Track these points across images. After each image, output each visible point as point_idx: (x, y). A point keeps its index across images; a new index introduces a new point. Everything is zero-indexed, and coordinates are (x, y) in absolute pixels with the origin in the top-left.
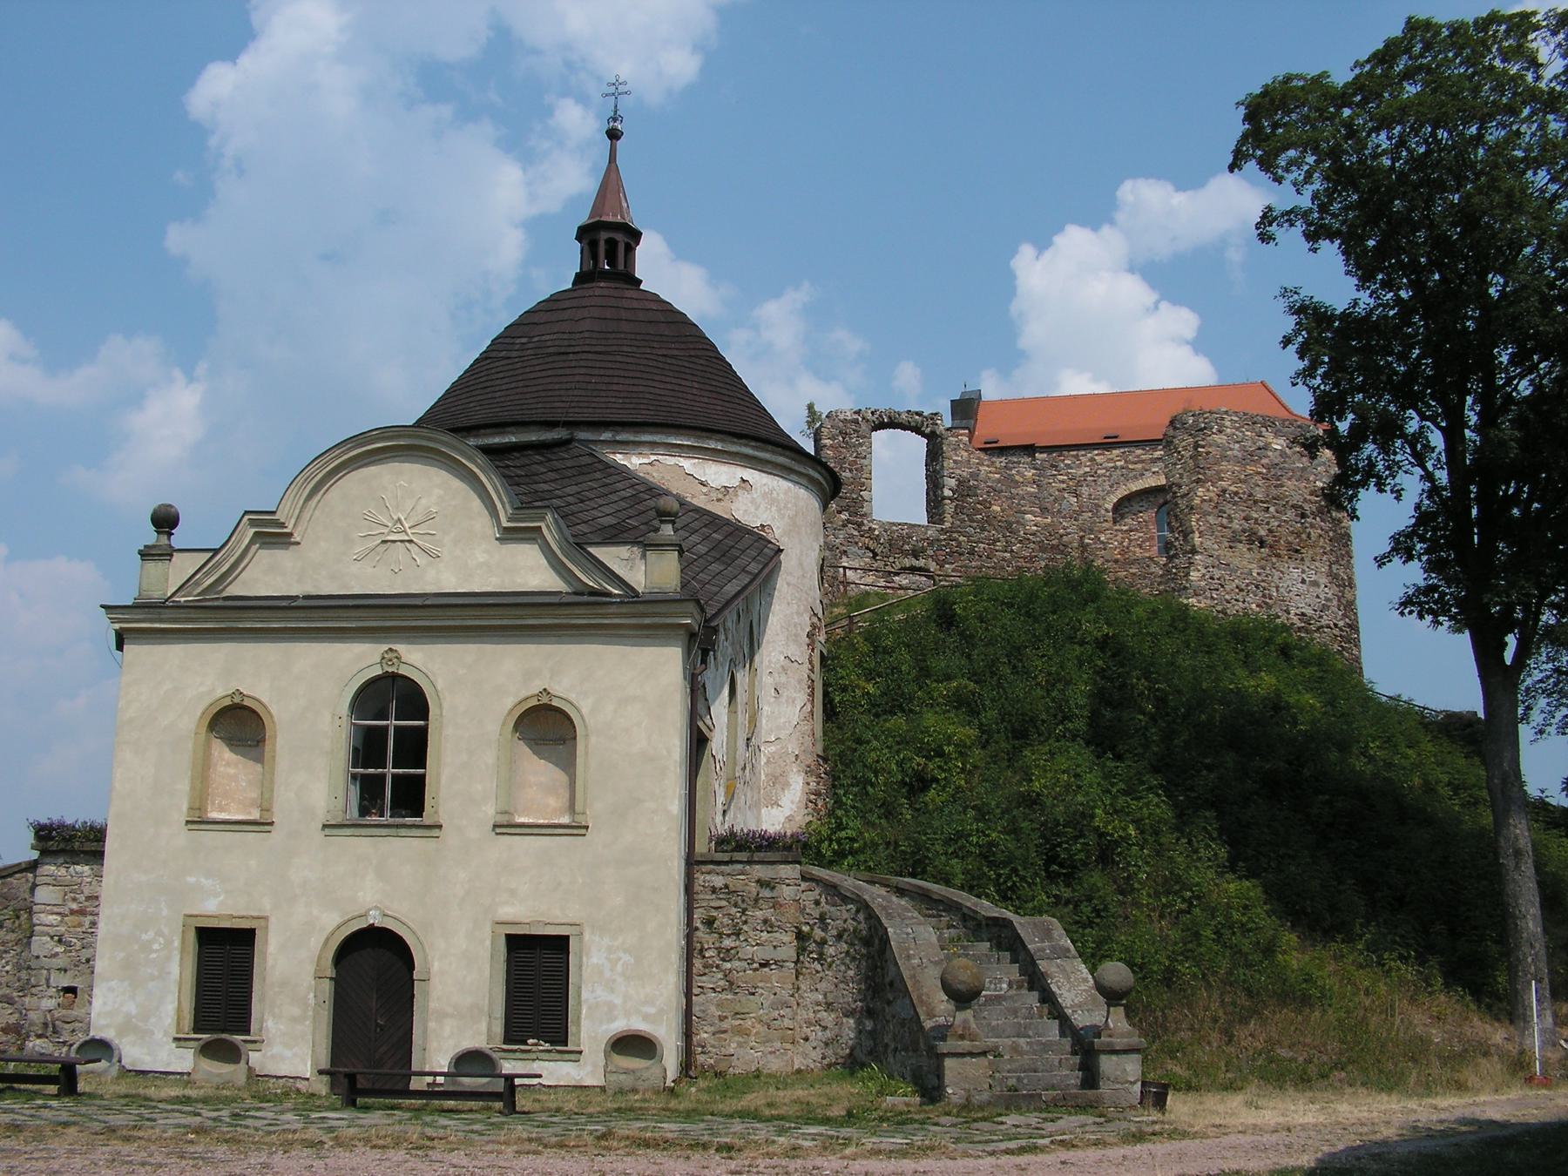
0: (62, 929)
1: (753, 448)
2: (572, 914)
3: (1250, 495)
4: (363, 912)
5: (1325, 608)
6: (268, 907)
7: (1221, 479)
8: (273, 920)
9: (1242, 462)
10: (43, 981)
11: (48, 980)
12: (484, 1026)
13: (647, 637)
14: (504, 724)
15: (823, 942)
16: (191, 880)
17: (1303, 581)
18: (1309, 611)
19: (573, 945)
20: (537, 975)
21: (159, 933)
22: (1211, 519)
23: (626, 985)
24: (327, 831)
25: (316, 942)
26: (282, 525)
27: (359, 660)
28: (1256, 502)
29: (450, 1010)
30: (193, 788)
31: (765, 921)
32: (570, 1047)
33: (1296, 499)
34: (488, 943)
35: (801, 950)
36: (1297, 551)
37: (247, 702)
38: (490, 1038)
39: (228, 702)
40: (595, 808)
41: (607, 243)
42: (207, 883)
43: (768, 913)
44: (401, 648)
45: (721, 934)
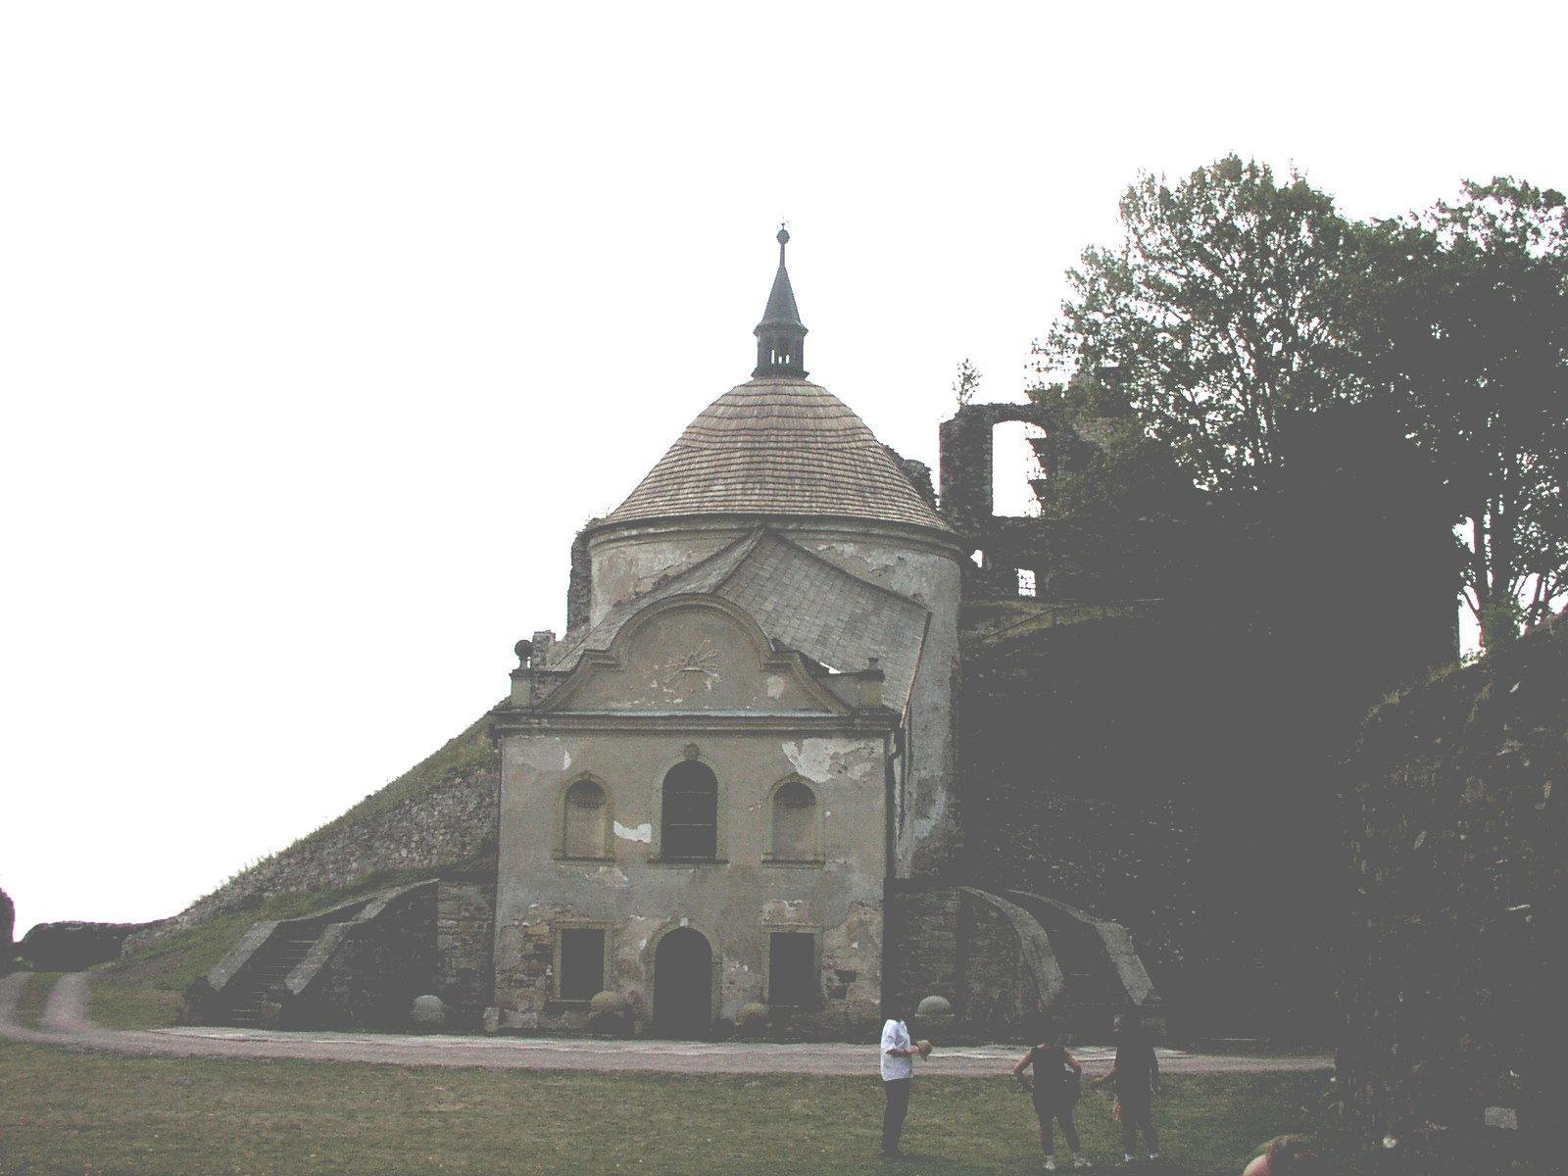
41: (781, 335)
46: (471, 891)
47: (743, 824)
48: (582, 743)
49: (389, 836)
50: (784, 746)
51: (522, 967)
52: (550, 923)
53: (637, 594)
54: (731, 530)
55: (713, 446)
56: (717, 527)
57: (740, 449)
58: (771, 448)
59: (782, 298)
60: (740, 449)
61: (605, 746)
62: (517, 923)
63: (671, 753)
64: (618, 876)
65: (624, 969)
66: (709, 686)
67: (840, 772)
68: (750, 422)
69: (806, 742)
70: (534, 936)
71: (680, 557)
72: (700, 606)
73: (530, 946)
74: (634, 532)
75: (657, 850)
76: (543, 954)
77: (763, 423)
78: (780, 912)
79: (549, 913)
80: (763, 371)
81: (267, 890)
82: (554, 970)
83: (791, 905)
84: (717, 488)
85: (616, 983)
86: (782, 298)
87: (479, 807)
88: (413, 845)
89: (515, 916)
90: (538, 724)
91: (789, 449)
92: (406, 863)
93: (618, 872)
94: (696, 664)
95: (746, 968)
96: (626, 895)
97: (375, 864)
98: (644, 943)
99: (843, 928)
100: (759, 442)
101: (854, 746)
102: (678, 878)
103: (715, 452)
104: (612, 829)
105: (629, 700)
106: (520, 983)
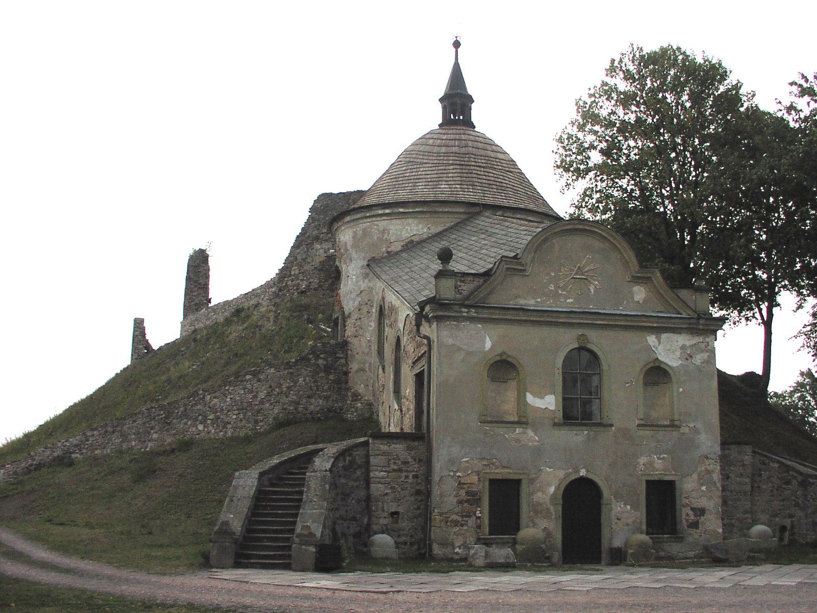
20: (661, 498)
37: (509, 359)
39: (498, 358)
41: (457, 102)
47: (620, 397)
48: (501, 329)
49: (185, 415)
50: (648, 338)
51: (456, 510)
52: (478, 473)
53: (388, 252)
54: (460, 213)
55: (431, 162)
56: (450, 210)
57: (452, 164)
58: (473, 166)
59: (457, 78)
60: (452, 164)
61: (517, 332)
62: (452, 474)
63: (568, 340)
64: (531, 436)
65: (538, 511)
66: (592, 291)
67: (687, 359)
68: (454, 149)
69: (664, 336)
70: (464, 484)
71: (422, 229)
72: (586, 230)
73: (463, 493)
74: (387, 211)
75: (560, 415)
76: (473, 499)
77: (463, 150)
78: (651, 463)
79: (479, 466)
80: (447, 122)
81: (74, 452)
82: (483, 512)
83: (659, 459)
84: (443, 186)
85: (532, 521)
86: (457, 78)
87: (269, 394)
88: (209, 422)
89: (452, 468)
90: (467, 312)
91: (484, 167)
92: (203, 434)
93: (530, 433)
94: (582, 274)
95: (629, 507)
96: (538, 452)
97: (174, 435)
98: (552, 489)
99: (695, 476)
100: (464, 161)
101: (696, 340)
102: (575, 437)
103: (432, 165)
104: (525, 398)
105: (533, 298)
106: (456, 523)
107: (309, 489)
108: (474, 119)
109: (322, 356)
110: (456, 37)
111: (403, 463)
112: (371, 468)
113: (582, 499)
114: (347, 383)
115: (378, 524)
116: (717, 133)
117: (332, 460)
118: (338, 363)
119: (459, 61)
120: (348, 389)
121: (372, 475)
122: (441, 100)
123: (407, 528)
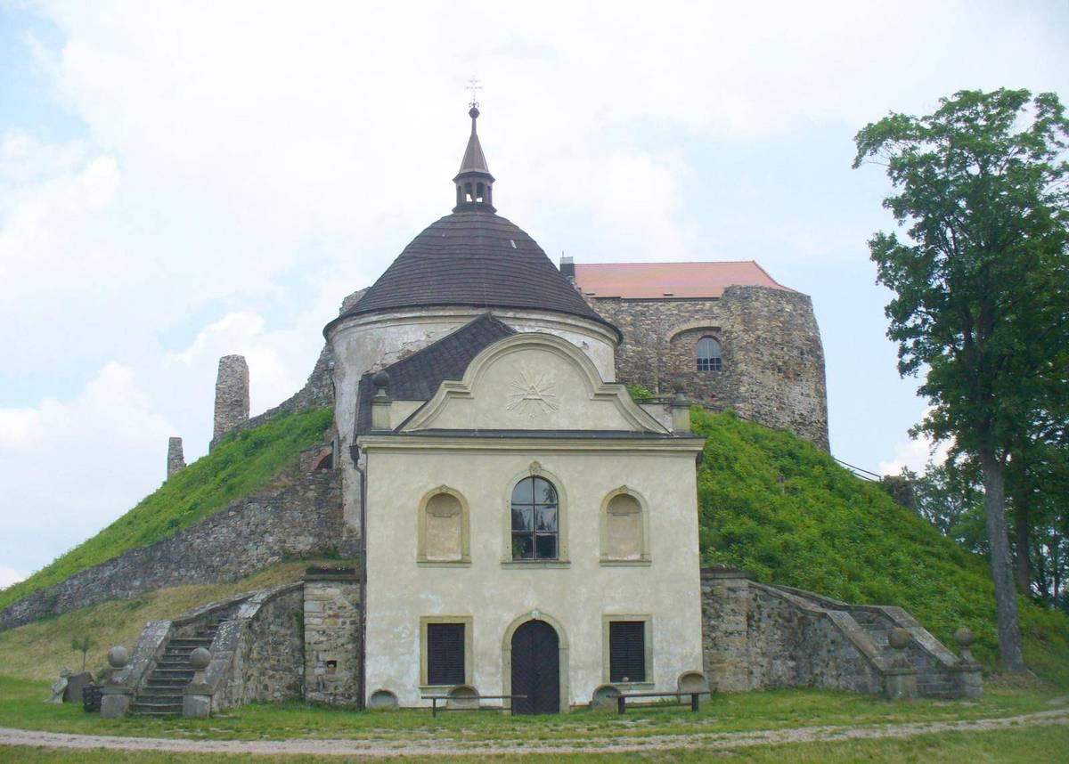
0: (324, 627)
1: (590, 324)
2: (646, 611)
3: (773, 340)
4: (527, 612)
5: (813, 410)
6: (471, 611)
7: (757, 330)
8: (475, 618)
9: (769, 319)
10: (314, 658)
11: (317, 658)
12: (600, 673)
13: (678, 457)
14: (602, 505)
15: (760, 620)
16: (423, 596)
17: (802, 394)
18: (805, 413)
19: (466, 626)
20: (627, 644)
21: (406, 628)
22: (751, 354)
23: (676, 650)
24: (421, 565)
25: (501, 631)
26: (465, 388)
27: (515, 467)
28: (776, 344)
29: (581, 665)
30: (420, 542)
31: (732, 610)
32: (648, 682)
33: (799, 343)
34: (600, 626)
35: (749, 625)
36: (799, 375)
37: (450, 492)
38: (604, 679)
39: (438, 492)
40: (655, 552)
41: (474, 180)
42: (433, 598)
43: (733, 606)
44: (541, 460)
45: (709, 618)
46: (335, 592)
47: (581, 526)
59: (474, 151)
80: (462, 207)
86: (474, 151)
94: (537, 394)
107: (219, 637)
108: (495, 204)
109: (312, 487)
110: (474, 104)
111: (339, 608)
112: (305, 614)
113: (535, 648)
114: (342, 517)
115: (312, 674)
116: (936, 175)
117: (259, 606)
118: (331, 495)
119: (478, 133)
120: (343, 524)
121: (306, 621)
122: (456, 180)
123: (345, 679)
